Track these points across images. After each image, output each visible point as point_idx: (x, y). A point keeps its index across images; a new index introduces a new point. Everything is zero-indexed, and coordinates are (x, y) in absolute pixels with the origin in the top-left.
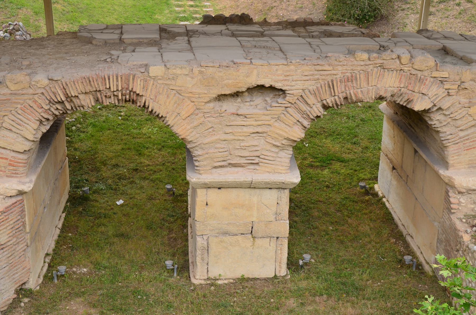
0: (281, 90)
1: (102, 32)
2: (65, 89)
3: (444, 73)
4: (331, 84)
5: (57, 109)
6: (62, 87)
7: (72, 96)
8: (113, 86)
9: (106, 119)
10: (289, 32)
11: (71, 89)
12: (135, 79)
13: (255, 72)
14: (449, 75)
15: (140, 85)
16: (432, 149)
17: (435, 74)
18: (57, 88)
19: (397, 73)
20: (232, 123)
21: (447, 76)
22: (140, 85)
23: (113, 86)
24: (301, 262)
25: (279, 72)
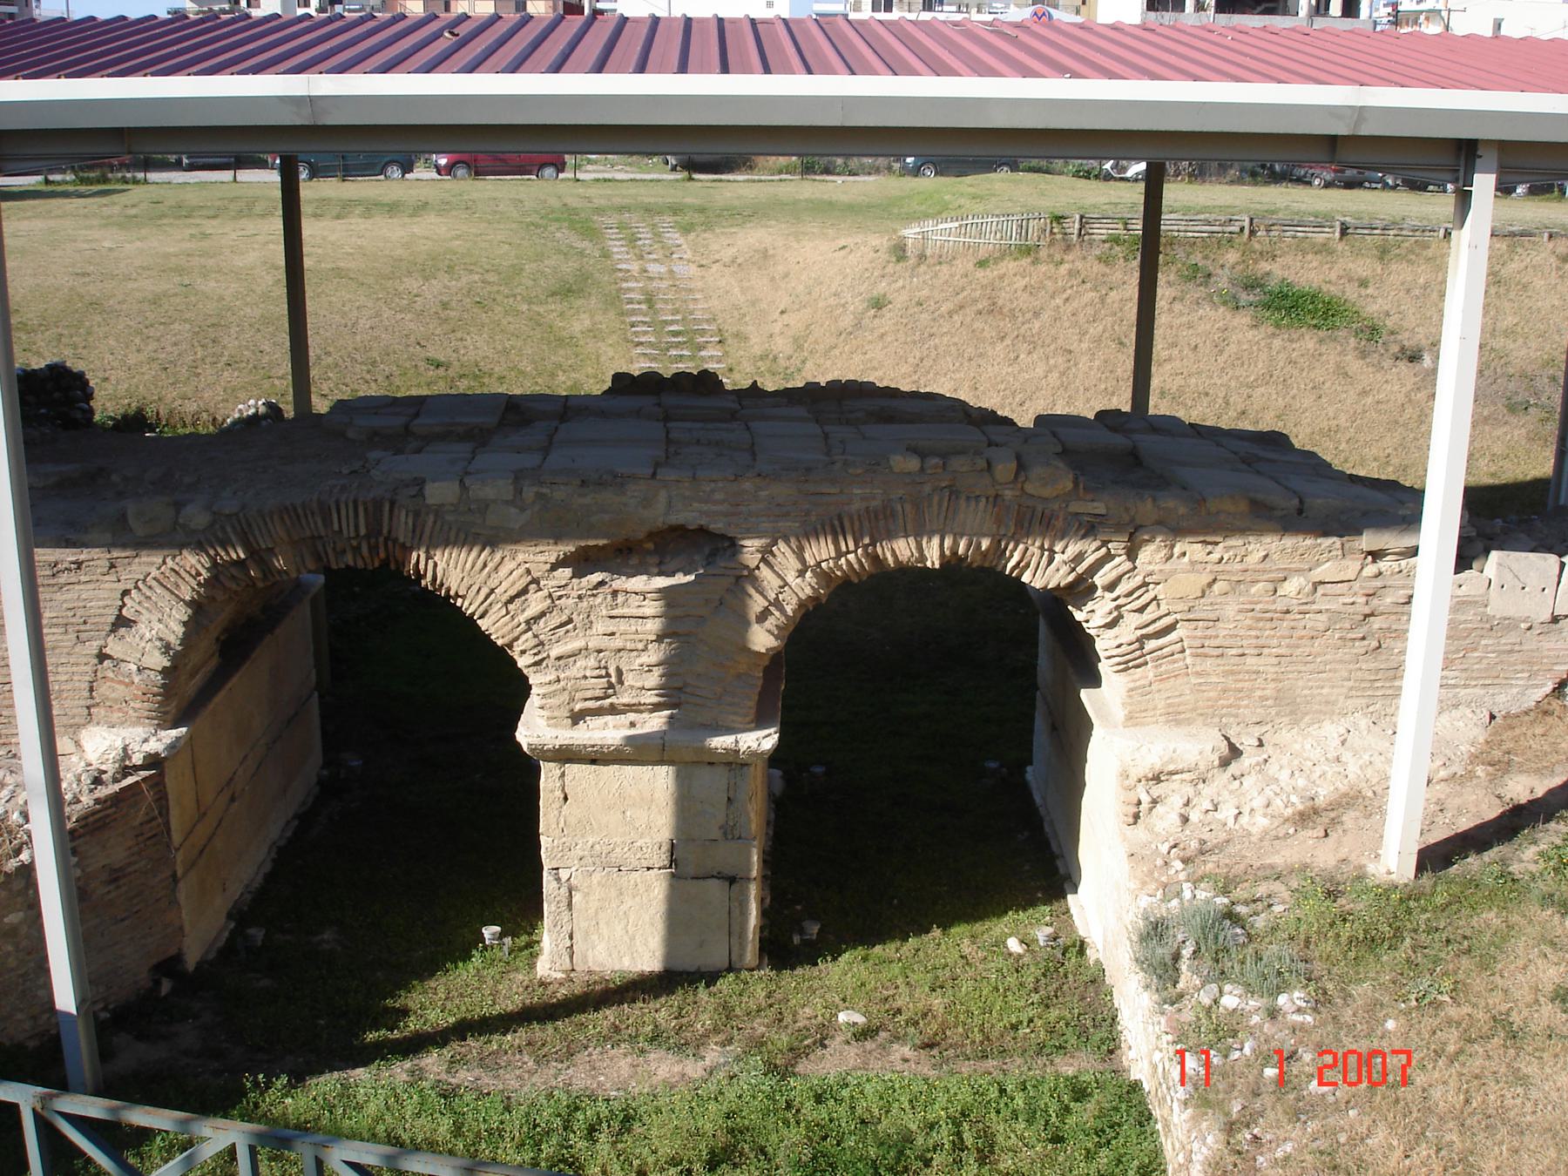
0: (723, 537)
1: (376, 414)
2: (246, 533)
3: (1095, 504)
4: (836, 523)
5: (233, 576)
6: (239, 528)
7: (260, 549)
8: (348, 525)
9: (1165, 1003)
10: (801, 411)
11: (257, 533)
12: (396, 510)
13: (663, 496)
14: (1108, 509)
15: (406, 523)
16: (752, 591)
17: (1075, 507)
18: (229, 529)
19: (987, 502)
20: (616, 611)
21: (1103, 512)
22: (406, 523)
23: (348, 525)
24: (796, 939)
25: (718, 496)
